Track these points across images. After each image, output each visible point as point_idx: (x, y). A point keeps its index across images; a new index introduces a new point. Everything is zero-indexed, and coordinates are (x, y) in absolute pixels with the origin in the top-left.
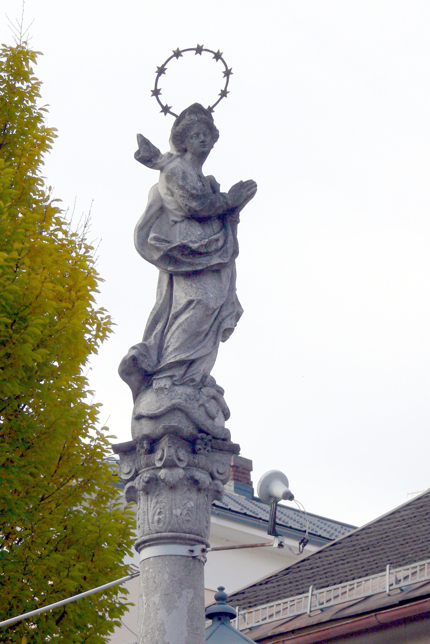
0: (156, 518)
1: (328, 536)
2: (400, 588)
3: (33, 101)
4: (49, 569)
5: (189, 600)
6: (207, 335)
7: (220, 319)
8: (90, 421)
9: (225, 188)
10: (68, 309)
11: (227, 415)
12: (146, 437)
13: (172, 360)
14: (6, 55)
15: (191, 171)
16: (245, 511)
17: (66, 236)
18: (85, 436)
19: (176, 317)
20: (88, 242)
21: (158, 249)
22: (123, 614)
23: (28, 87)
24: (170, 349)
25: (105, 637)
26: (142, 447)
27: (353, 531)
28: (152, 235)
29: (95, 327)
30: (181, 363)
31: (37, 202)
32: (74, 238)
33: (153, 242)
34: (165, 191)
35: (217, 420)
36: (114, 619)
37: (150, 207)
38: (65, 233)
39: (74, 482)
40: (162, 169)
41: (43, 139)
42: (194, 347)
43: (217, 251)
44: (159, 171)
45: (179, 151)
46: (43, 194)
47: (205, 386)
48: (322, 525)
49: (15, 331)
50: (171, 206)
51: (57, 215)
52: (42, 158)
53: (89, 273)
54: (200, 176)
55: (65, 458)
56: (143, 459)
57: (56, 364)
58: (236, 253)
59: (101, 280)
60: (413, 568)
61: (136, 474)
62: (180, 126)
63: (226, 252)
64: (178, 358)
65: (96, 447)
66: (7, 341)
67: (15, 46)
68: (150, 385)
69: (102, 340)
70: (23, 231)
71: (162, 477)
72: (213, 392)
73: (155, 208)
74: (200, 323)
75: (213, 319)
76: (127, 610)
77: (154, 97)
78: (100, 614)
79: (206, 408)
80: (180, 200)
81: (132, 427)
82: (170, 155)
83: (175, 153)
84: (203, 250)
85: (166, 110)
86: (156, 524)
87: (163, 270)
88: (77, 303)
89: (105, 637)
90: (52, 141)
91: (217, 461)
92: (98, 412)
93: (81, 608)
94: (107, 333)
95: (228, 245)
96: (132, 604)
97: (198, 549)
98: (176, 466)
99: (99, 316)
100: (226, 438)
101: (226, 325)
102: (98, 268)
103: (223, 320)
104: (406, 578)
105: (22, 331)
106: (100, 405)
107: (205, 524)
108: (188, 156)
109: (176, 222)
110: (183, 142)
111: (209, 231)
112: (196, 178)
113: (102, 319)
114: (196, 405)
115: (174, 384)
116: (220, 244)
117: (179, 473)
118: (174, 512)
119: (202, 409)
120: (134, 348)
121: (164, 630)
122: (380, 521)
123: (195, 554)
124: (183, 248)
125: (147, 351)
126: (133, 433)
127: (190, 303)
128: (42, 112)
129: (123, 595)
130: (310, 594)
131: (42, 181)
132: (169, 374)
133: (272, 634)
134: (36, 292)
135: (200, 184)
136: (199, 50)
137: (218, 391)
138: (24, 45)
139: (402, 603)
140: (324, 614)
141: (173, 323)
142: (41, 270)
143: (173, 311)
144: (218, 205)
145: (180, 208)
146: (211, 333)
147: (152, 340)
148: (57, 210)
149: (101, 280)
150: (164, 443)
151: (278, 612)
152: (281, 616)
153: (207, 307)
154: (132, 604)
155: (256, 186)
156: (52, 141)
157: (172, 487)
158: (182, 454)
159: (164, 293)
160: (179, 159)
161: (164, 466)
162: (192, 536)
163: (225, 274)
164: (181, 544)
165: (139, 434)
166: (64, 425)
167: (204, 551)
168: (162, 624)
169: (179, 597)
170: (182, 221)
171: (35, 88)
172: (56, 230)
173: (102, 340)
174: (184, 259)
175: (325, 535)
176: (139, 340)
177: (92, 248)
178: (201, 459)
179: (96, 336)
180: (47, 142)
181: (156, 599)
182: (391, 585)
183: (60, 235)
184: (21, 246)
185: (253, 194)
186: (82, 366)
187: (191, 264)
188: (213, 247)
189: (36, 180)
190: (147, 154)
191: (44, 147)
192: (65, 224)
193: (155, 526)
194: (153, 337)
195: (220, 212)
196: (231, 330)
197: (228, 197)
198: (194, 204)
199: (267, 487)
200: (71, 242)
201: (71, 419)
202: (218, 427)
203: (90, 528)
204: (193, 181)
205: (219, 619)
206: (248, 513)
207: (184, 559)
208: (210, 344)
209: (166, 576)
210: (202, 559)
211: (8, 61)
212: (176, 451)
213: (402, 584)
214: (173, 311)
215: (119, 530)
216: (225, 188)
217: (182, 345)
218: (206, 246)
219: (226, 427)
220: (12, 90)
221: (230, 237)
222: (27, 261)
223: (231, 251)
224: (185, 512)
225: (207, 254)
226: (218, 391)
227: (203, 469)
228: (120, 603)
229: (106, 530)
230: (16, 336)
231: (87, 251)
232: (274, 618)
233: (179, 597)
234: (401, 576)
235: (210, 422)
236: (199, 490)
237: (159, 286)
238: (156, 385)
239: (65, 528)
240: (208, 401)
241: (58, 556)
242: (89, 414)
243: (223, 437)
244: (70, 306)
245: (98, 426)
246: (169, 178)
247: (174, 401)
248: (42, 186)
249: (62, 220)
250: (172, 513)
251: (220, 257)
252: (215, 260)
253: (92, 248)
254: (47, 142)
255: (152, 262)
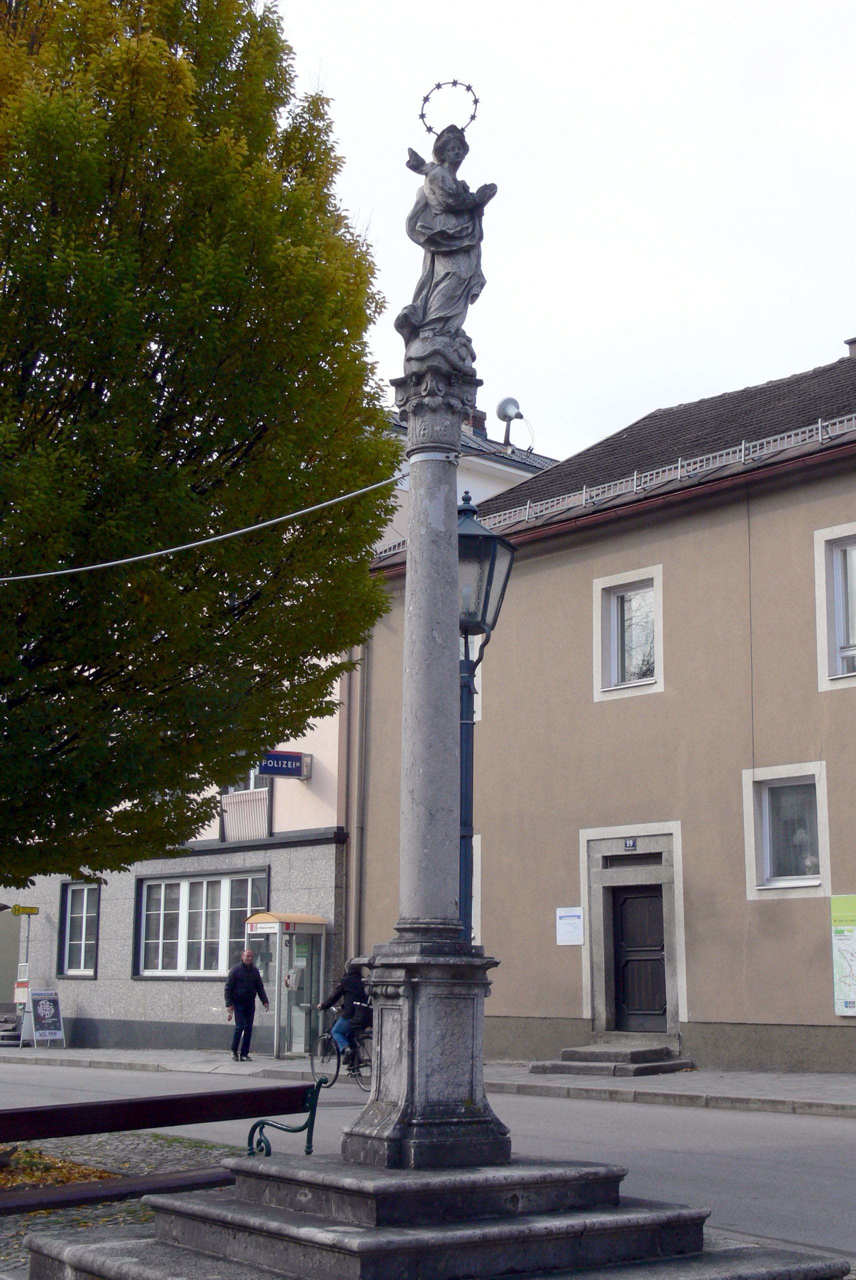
0: (422, 433)
1: (541, 467)
2: (593, 502)
3: (328, 136)
4: (341, 479)
5: (446, 493)
6: (459, 298)
7: (469, 287)
8: (370, 375)
9: (473, 189)
10: (353, 290)
11: (474, 358)
12: (414, 374)
13: (434, 317)
14: (308, 101)
15: (448, 176)
16: (481, 448)
17: (353, 237)
18: (366, 385)
19: (437, 285)
20: (369, 242)
21: (423, 234)
22: (394, 513)
23: (324, 125)
24: (432, 309)
25: (381, 529)
26: (412, 381)
27: (558, 464)
28: (419, 224)
29: (374, 304)
30: (439, 320)
31: (330, 212)
32: (358, 239)
33: (420, 229)
34: (429, 191)
35: (466, 361)
36: (388, 517)
37: (417, 203)
38: (352, 234)
39: (357, 419)
40: (426, 174)
41: (335, 165)
42: (450, 307)
43: (467, 236)
44: (424, 176)
45: (439, 161)
46: (335, 206)
47: (458, 336)
48: (536, 460)
49: (316, 306)
50: (433, 202)
51: (346, 221)
52: (334, 179)
53: (370, 265)
54: (455, 180)
55: (352, 401)
56: (412, 390)
57: (346, 331)
58: (481, 238)
59: (379, 270)
60: (603, 488)
61: (407, 401)
62: (440, 142)
63: (474, 237)
64: (438, 316)
65: (375, 393)
66: (310, 313)
67: (314, 94)
68: (417, 336)
69: (379, 314)
70: (321, 231)
71: (426, 403)
72: (464, 340)
73: (422, 204)
74: (455, 289)
75: (464, 287)
76: (397, 510)
77: (421, 120)
78: (378, 513)
79: (459, 353)
80: (440, 198)
81: (405, 367)
82: (433, 164)
83: (436, 162)
84: (457, 235)
85: (430, 129)
86: (422, 437)
87: (427, 251)
88: (360, 286)
89: (381, 529)
90: (341, 166)
91: (467, 392)
92: (376, 368)
93: (364, 509)
94: (383, 309)
95: (476, 232)
96: (401, 506)
97: (452, 456)
98: (437, 395)
99: (377, 297)
100: (473, 373)
101: (473, 292)
102: (375, 260)
103: (472, 288)
104: (598, 495)
105: (321, 305)
106: (378, 362)
107: (458, 437)
108: (446, 165)
109: (437, 215)
110: (442, 154)
111: (461, 221)
112: (451, 181)
113: (379, 299)
114: (452, 351)
115: (435, 335)
116: (470, 230)
117: (439, 400)
118: (435, 428)
119: (456, 353)
120: (406, 308)
121: (428, 514)
122: (579, 455)
123: (450, 460)
124: (442, 233)
125: (415, 311)
126: (405, 371)
127: (447, 274)
128: (334, 144)
129: (394, 500)
130: (528, 506)
131: (334, 196)
132: (431, 327)
133: (278, 1174)
134: (331, 277)
135: (455, 186)
136: (455, 83)
137: (468, 340)
138: (321, 93)
139: (594, 512)
140: (538, 520)
141: (435, 290)
142: (334, 261)
143: (435, 281)
144: (468, 201)
145: (440, 204)
146: (463, 297)
147: (419, 302)
148: (346, 218)
149: (379, 270)
150: (428, 378)
151: (505, 520)
152: (507, 522)
153: (460, 278)
154: (401, 506)
155: (496, 188)
156: (341, 166)
157: (434, 410)
158: (441, 386)
159: (428, 267)
160: (439, 167)
161: (428, 395)
162: (448, 446)
163: (473, 254)
164: (439, 451)
165: (409, 372)
166: (351, 376)
167: (456, 457)
168: (426, 510)
169: (439, 490)
170: (441, 214)
171: (329, 126)
172: (345, 232)
173: (379, 314)
174: (443, 242)
175: (538, 466)
176: (410, 302)
177: (371, 246)
178: (455, 390)
179: (375, 312)
180: (338, 167)
181: (422, 491)
182: (587, 500)
183: (348, 236)
184: (320, 242)
185: (494, 194)
186: (364, 334)
187: (448, 246)
188: (465, 233)
189: (330, 195)
190: (415, 163)
191: (336, 170)
192: (352, 228)
193: (421, 439)
194: (419, 300)
195: (470, 207)
196: (477, 295)
197: (476, 196)
198: (450, 201)
199: (504, 409)
200: (357, 241)
201: (356, 372)
202: (467, 367)
203: (370, 450)
204: (449, 183)
205: (465, 514)
206: (483, 449)
207: (442, 464)
208: (462, 305)
209: (429, 475)
210: (456, 463)
211: (309, 106)
212: (437, 384)
213: (595, 499)
214: (435, 281)
215: (392, 453)
216: (473, 189)
217: (441, 305)
218: (460, 232)
219: (473, 367)
220: (312, 127)
221: (477, 226)
222: (324, 254)
223: (477, 236)
224: (443, 429)
225: (461, 238)
226: (468, 340)
227: (456, 397)
228: (392, 506)
229: (381, 453)
230: (317, 309)
231: (368, 249)
232: (502, 524)
233: (439, 490)
234: (594, 494)
235: (462, 363)
236: (453, 413)
237: (424, 262)
238: (422, 335)
239: (352, 451)
240: (460, 348)
241: (348, 471)
242: (370, 369)
243: (471, 374)
244: (356, 288)
245: (376, 378)
246: (432, 181)
247: (435, 347)
248: (335, 200)
249: (349, 225)
250: (433, 429)
251: (469, 240)
252: (466, 243)
253: (371, 246)
254: (338, 167)
255: (419, 244)
